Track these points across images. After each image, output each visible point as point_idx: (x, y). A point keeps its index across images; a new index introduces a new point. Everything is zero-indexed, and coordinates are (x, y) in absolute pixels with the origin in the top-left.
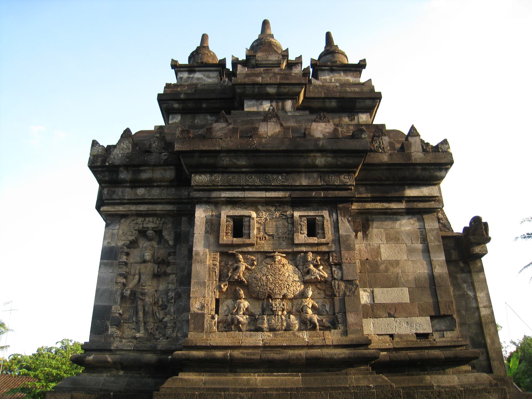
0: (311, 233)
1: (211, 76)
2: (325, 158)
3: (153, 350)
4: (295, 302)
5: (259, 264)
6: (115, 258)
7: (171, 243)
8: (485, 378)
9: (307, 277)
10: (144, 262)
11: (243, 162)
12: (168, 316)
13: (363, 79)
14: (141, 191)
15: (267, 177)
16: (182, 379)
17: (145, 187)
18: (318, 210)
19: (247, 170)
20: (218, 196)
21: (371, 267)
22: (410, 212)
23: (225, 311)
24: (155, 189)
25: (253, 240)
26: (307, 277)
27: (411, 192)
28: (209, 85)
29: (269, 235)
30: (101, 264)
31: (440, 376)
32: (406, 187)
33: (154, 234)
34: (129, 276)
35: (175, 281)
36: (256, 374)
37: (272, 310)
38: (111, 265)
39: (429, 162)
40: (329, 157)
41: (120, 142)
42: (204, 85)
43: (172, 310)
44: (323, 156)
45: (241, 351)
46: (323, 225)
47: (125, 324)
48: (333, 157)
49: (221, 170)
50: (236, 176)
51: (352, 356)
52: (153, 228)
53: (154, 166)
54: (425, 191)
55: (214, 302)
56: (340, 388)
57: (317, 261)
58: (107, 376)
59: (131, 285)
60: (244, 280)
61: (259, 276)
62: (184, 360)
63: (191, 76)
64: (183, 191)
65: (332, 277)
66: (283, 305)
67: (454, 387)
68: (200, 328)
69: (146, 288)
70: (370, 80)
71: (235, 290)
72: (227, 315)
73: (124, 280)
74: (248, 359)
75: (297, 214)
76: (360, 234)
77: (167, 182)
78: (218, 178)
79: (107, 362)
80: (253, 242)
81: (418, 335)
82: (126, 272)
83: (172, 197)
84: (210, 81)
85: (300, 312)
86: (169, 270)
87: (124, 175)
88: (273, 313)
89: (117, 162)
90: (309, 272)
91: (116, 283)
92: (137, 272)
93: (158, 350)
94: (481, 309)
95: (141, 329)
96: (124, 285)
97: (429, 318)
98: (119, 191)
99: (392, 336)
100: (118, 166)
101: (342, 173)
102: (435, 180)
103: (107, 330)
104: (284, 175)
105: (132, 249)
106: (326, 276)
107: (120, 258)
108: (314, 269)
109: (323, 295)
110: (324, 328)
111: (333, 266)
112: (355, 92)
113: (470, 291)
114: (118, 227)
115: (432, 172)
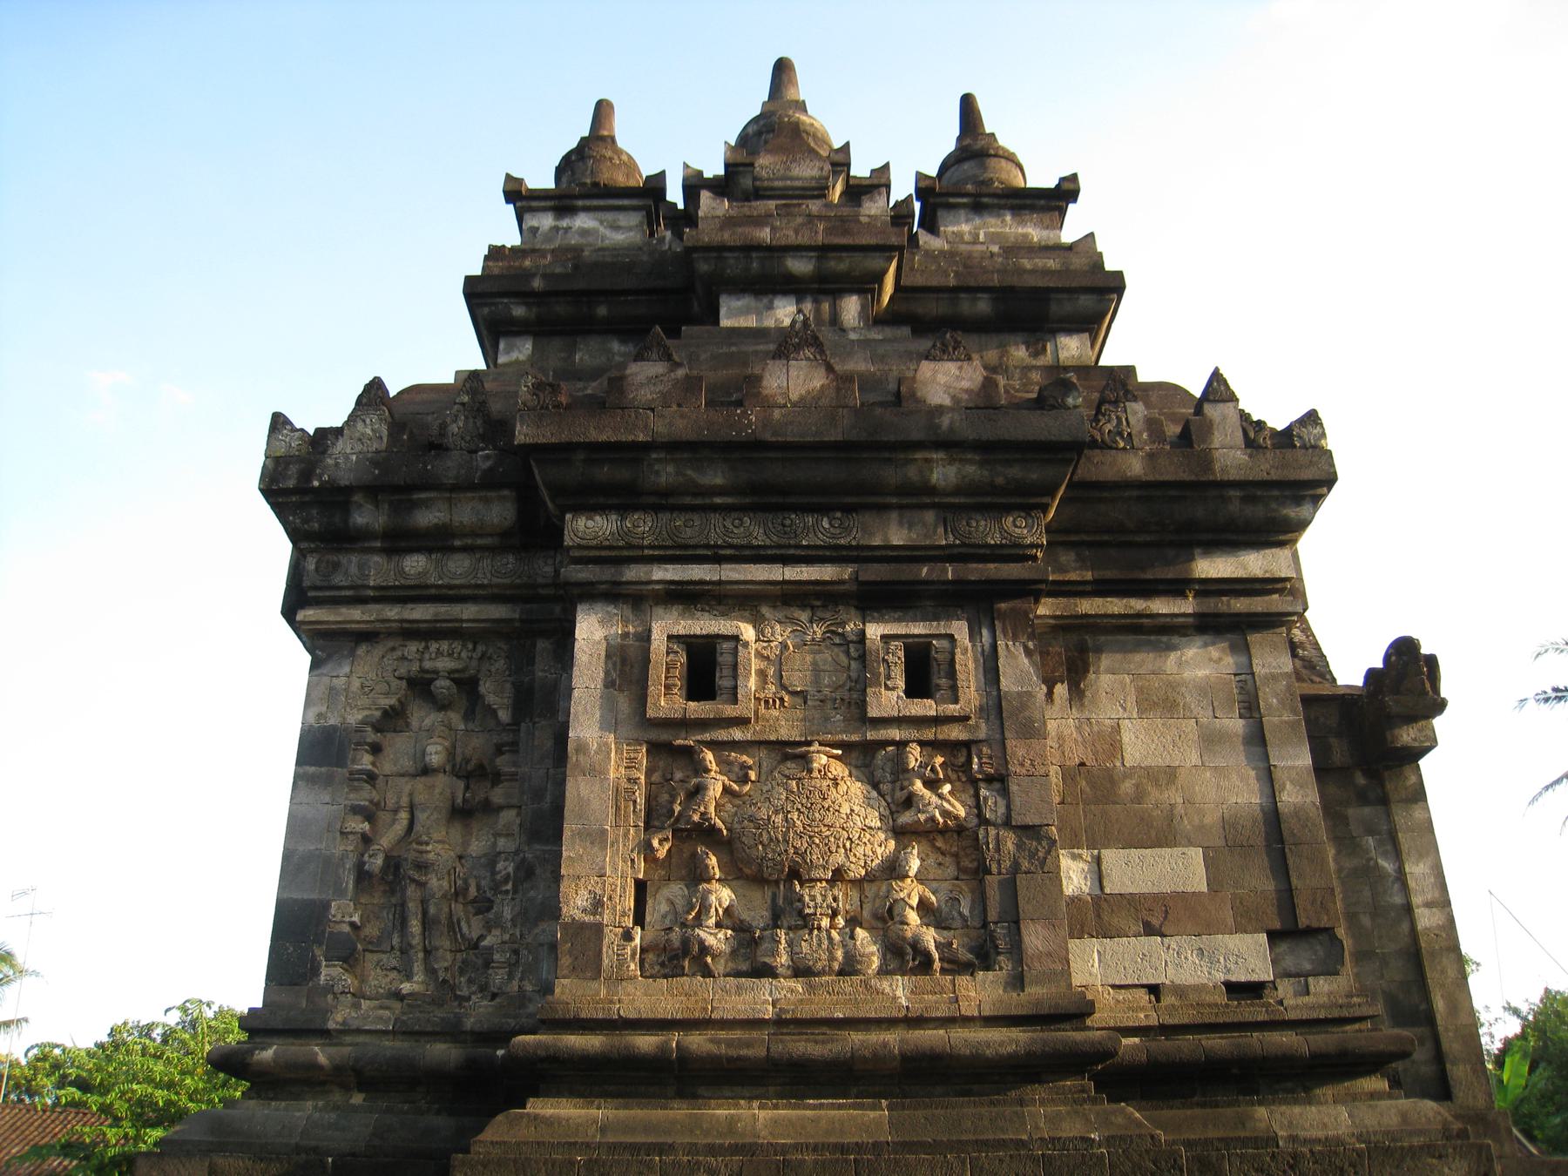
0: (918, 686)
1: (623, 223)
2: (957, 464)
3: (452, 1032)
4: (870, 890)
5: (763, 778)
6: (340, 761)
7: (504, 716)
8: (1431, 1114)
9: (906, 818)
10: (426, 771)
11: (715, 477)
12: (496, 932)
13: (1070, 233)
14: (415, 564)
15: (788, 522)
16: (536, 1117)
17: (429, 551)
18: (937, 618)
19: (729, 500)
20: (644, 578)
21: (1093, 786)
22: (1208, 626)
23: (664, 917)
24: (457, 556)
25: (744, 708)
26: (906, 818)
27: (1212, 567)
28: (615, 250)
29: (794, 693)
30: (297, 777)
31: (1297, 1110)
32: (1197, 551)
33: (454, 690)
34: (381, 814)
35: (516, 829)
36: (756, 1104)
37: (800, 913)
38: (328, 781)
39: (1266, 477)
40: (971, 462)
41: (353, 417)
42: (600, 249)
43: (507, 913)
44: (951, 461)
45: (711, 1033)
46: (952, 662)
47: (368, 956)
48: (982, 464)
49: (652, 500)
50: (697, 519)
51: (1037, 1048)
52: (451, 672)
53: (454, 488)
54: (1253, 563)
55: (631, 891)
56: (1001, 1144)
57: (933, 770)
58: (315, 1107)
59: (386, 840)
60: (719, 824)
61: (763, 814)
62: (542, 1060)
63: (564, 223)
64: (541, 562)
65: (980, 815)
66: (835, 899)
67: (1339, 1141)
68: (590, 965)
69: (429, 848)
70: (1092, 235)
71: (694, 855)
72: (670, 929)
73: (366, 826)
74: (730, 1060)
75: (874, 631)
76: (1061, 690)
77: (491, 535)
78: (643, 526)
79: (314, 1066)
80: (746, 714)
81: (1233, 988)
82: (371, 801)
83: (507, 581)
84: (619, 238)
85: (885, 919)
86: (498, 795)
87: (364, 517)
88: (806, 922)
89: (345, 479)
90: (909, 801)
91: (342, 833)
92: (405, 801)
93: (465, 1032)
94: (1418, 912)
95: (416, 969)
96: (366, 840)
97: (1263, 937)
98: (350, 562)
99: (1154, 990)
100: (349, 490)
101: (1008, 509)
102: (1281, 532)
103: (315, 972)
104: (838, 515)
105: (389, 735)
106: (962, 812)
107: (354, 761)
108: (927, 793)
109: (951, 871)
110: (956, 966)
111: (982, 785)
112: (1047, 272)
113: (1386, 859)
114: (347, 669)
115: (1274, 505)
